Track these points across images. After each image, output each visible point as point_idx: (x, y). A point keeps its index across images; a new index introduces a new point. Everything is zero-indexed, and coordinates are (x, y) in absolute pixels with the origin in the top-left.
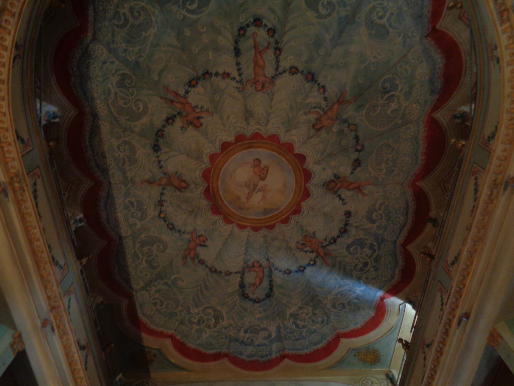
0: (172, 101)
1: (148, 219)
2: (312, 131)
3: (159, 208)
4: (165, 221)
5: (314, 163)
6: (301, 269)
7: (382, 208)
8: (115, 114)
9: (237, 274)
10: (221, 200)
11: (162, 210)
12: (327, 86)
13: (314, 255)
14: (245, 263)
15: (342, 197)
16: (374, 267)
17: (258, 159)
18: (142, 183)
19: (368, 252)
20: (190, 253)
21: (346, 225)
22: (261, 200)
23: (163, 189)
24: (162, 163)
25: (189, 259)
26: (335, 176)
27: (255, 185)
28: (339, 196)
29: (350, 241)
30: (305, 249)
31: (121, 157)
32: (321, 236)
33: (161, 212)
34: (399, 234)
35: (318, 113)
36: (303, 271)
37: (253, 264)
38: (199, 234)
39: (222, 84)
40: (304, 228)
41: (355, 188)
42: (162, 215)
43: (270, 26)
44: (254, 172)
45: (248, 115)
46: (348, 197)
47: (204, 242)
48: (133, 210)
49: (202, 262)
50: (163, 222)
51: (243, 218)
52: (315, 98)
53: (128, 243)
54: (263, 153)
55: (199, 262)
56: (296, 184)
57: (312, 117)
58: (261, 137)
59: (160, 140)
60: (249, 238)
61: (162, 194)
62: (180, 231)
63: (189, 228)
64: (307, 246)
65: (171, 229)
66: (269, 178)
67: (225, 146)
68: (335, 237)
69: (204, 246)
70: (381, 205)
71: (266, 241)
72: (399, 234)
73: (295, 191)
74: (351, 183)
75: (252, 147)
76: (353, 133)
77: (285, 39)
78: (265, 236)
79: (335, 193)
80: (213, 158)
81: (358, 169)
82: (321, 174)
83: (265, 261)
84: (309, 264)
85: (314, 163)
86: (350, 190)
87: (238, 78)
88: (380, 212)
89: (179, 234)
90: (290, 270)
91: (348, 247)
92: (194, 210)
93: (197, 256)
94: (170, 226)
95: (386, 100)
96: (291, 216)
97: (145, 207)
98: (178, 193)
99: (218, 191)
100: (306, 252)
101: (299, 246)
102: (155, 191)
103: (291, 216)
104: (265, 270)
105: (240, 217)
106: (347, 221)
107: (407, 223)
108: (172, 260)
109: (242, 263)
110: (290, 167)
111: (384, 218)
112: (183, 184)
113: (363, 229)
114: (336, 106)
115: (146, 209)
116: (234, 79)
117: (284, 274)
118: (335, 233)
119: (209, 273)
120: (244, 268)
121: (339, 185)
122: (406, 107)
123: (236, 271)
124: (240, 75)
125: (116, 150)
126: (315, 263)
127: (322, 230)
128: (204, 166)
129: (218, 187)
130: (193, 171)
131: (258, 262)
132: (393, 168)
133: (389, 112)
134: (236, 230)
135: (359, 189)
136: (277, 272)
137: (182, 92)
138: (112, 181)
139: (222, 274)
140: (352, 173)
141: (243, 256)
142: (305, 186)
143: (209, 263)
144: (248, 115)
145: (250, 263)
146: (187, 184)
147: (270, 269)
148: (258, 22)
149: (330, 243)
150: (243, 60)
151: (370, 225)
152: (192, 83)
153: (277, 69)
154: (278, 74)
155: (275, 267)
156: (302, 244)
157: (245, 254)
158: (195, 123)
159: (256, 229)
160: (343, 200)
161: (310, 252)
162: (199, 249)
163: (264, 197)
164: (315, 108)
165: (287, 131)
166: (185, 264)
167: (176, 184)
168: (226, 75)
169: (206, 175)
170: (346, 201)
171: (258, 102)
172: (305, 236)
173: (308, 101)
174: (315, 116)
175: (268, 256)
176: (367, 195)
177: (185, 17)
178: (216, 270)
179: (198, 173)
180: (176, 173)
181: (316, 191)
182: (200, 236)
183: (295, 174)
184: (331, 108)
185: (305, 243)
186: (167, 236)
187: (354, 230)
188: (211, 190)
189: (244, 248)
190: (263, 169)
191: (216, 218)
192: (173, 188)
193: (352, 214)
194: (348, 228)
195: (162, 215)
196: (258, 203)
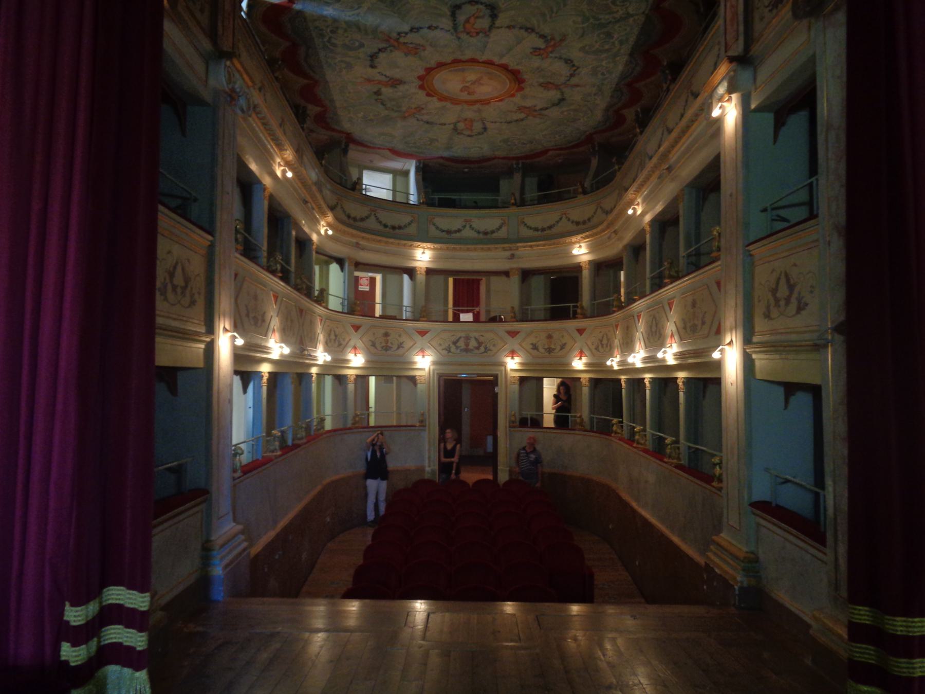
54: (465, 96)
172: (416, 54)
186: (576, 55)
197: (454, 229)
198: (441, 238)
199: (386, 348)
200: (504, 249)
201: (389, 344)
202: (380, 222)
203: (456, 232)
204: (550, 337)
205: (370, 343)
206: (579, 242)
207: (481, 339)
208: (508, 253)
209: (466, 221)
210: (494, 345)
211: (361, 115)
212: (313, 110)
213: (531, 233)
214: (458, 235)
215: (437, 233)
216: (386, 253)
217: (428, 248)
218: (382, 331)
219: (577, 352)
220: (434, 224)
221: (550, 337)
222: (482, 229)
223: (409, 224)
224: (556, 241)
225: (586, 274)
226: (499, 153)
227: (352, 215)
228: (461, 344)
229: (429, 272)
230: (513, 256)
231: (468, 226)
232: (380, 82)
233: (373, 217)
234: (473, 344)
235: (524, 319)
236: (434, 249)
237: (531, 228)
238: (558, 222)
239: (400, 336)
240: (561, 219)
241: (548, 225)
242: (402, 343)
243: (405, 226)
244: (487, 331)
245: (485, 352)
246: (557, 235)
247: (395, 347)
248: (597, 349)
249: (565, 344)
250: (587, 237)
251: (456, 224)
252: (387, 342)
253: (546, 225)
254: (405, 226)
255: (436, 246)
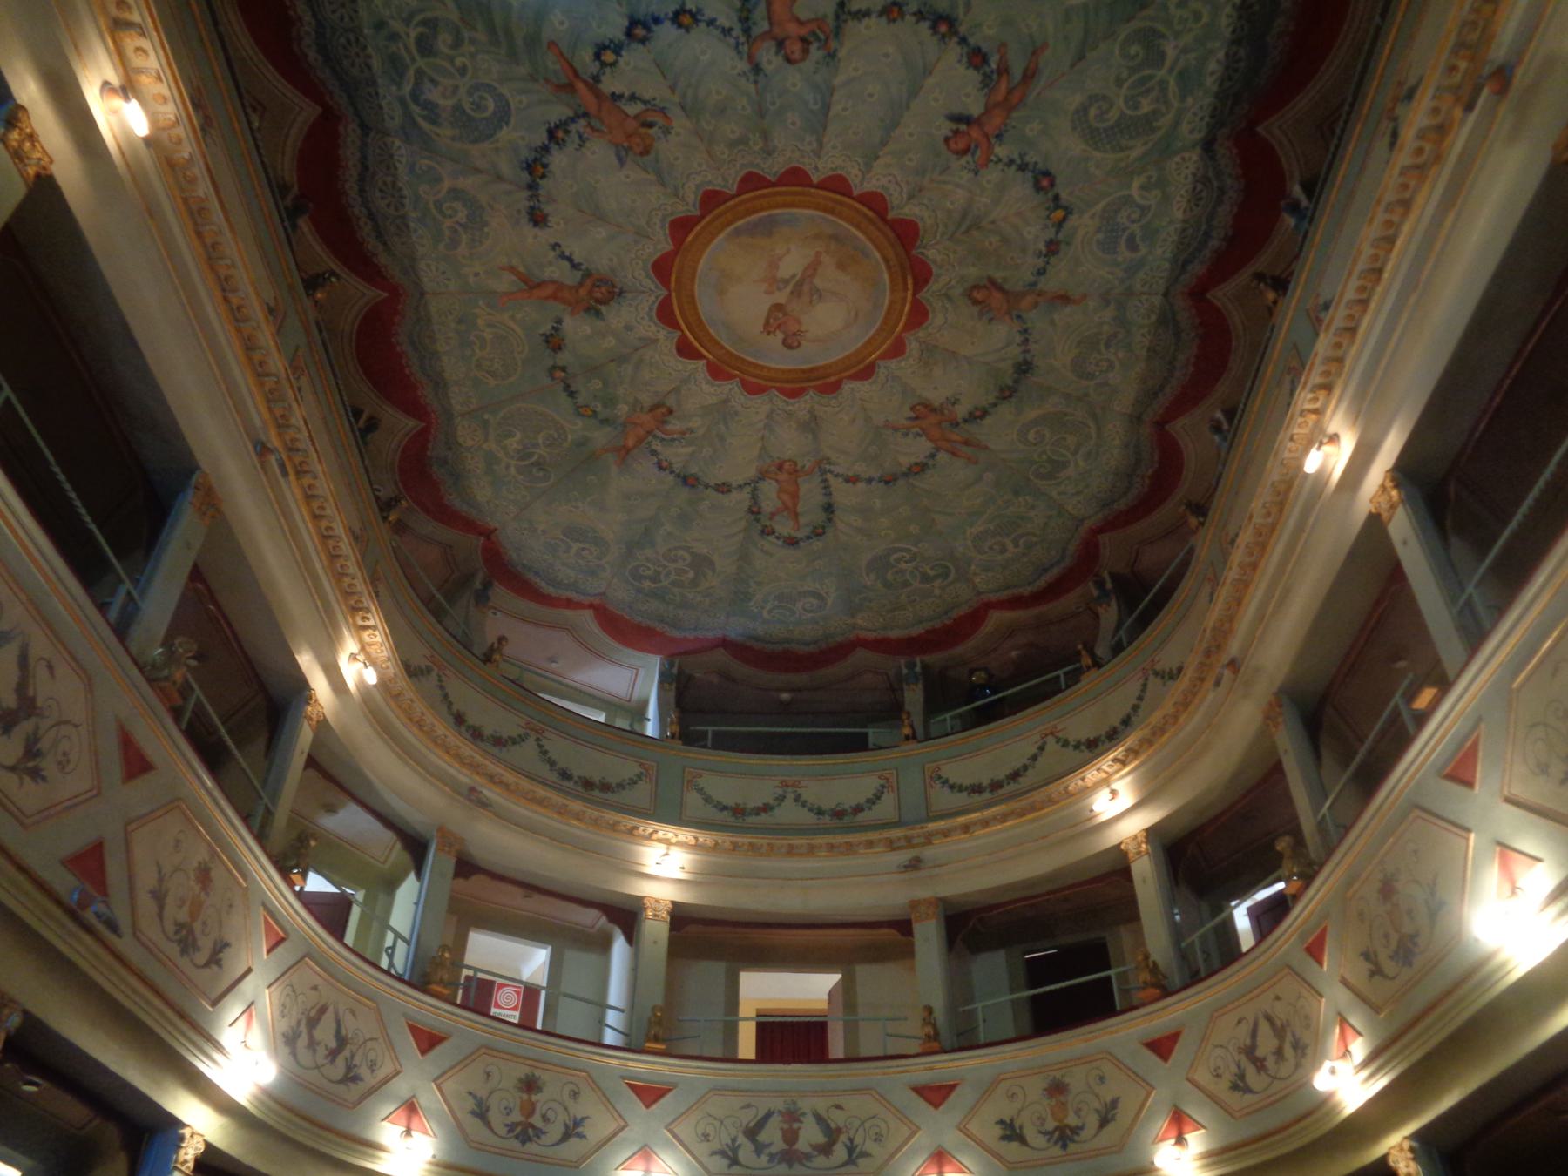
0: (966, 443)
1: (1103, 203)
2: (671, 402)
3: (1061, 236)
4: (1056, 198)
5: (656, 341)
6: (640, 32)
7: (447, 233)
8: (1092, 425)
9: (864, 7)
10: (886, 261)
11: (1053, 230)
12: (656, 470)
13: (609, 85)
14: (832, 55)
15: (566, 264)
16: (394, 37)
17: (790, 347)
18: (1084, 297)
19: (433, 95)
20: (1010, 92)
21: (532, 187)
22: (780, 259)
23: (1034, 284)
24: (1018, 339)
25: (1017, 72)
26: (598, 314)
27: (797, 292)
28: (575, 266)
29: (505, 134)
30: (639, 107)
31: (1112, 350)
32: (599, 151)
33: (1060, 225)
34: (364, 158)
35: (665, 433)
36: (634, 22)
37: (806, 52)
38: (968, 158)
39: (860, 468)
40: (652, 177)
41: (539, 285)
42: (1060, 214)
43: (771, 538)
44: (799, 323)
45: (811, 425)
46: (550, 263)
47: (956, 132)
48: (1135, 228)
49: (977, 58)
50: (1063, 195)
51: (832, 212)
52: (677, 454)
53: (1192, 129)
54: (775, 357)
55: (985, 59)
56: (693, 297)
57: (675, 425)
58: (782, 391)
59: (1010, 383)
60: (815, 145)
61: (1041, 272)
62: (1023, 167)
63: (992, 175)
64: (636, 117)
65: (1047, 174)
66: (765, 307)
67: (867, 373)
68: (554, 148)
69: (957, 118)
70: (454, 243)
71: (765, 136)
72: (364, 158)
73: (692, 280)
74: (554, 297)
75: (803, 371)
76: (581, 400)
77: (743, 523)
78: (769, 152)
79: (588, 274)
80: (897, 350)
81: (546, 328)
82: (634, 316)
83: (764, 65)
84: (617, 50)
85: (656, 341)
86: (553, 282)
87: (829, 476)
88: (448, 223)
89: (1027, 159)
90: (680, 26)
91: (503, 115)
92: (967, 232)
93: (987, 82)
94: (1045, 183)
95: (531, 455)
96: (697, 213)
97: (1100, 236)
98: (998, 275)
99: (892, 280)
100: (633, 98)
101: (660, 120)
102: (1059, 277)
103: (697, 213)
104: (765, 26)
105: (840, 215)
106: (535, 197)
107: (356, 188)
108: (1073, 66)
109: (842, 54)
110: (712, 332)
111: (432, 206)
112: (978, 296)
113: (481, 172)
114: (630, 443)
115: (1098, 230)
116: (837, 476)
117: (700, 11)
118: (558, 160)
119: (961, 11)
120: (838, 32)
121: (583, 292)
122: (486, 440)
123: (866, 21)
124: (825, 481)
125: (1117, 364)
126: (597, 56)
127: (592, 166)
128: (921, 334)
129: (893, 291)
130: (950, 323)
131: (789, 60)
132: (463, 328)
133: (519, 435)
134: (853, 174)
135: (531, 284)
136: (723, 21)
137: (942, 457)
138: (1157, 300)
139: (913, 7)
140: (560, 321)
141: (837, 81)
142: (668, 288)
143: (954, 51)
144: (811, 425)
145: (816, 53)
146: (970, 297)
147: (747, 31)
148: (792, 542)
149: (563, 125)
150: (819, 499)
151: (468, 183)
152: (921, 468)
153: (755, 489)
154: (753, 485)
155: (732, 41)
156: (650, 125)
157: (832, 90)
158: (924, 412)
159: (795, 176)
160: (563, 256)
161: (621, 96)
162: (976, 110)
163: (774, 265)
164: (673, 440)
165: (726, 401)
166: (1034, 53)
167: (997, 295)
168: (852, 480)
169: (919, 315)
170: (552, 254)
171: (790, 443)
172: (646, 152)
173: (690, 450)
174: (669, 427)
175: (756, 82)
176: (503, 269)
177: (916, 545)
178: (934, 28)
179: (937, 319)
180: (991, 320)
181: (637, 275)
182: (965, 151)
183: (701, 322)
184: (640, 441)
185: (643, 130)
186: (1065, 147)
187: (506, 168)
188: (910, 286)
189: (831, 114)
190: (779, 327)
191: (910, 211)
192: (1006, 287)
193: (524, 219)
194: (525, 177)
195: (1060, 214)
196: (788, 251)
197: (751, 805)
198: (722, 818)
199: (525, 1133)
200: (891, 845)
201: (536, 1120)
202: (552, 764)
203: (759, 811)
204: (1057, 1089)
205: (470, 1104)
206: (1106, 782)
207: (837, 1118)
208: (904, 856)
209: (784, 785)
210: (878, 1139)
211: (513, 443)
212: (398, 425)
213: (961, 799)
214: (764, 817)
215: (711, 813)
216: (557, 840)
217: (679, 844)
218: (522, 1071)
219: (1162, 1124)
220: (700, 791)
221: (1057, 1089)
222: (828, 804)
223: (633, 782)
224: (1038, 796)
225: (1144, 870)
226: (867, 624)
227: (471, 719)
228: (772, 1134)
229: (680, 917)
230: (915, 865)
231: (790, 797)
232: (557, 292)
233: (531, 741)
234: (810, 1135)
235: (966, 1041)
236: (696, 847)
237: (961, 789)
238: (1034, 758)
239: (575, 1095)
240: (1042, 748)
241: (1007, 771)
242: (578, 1123)
243: (621, 786)
244: (857, 1090)
245: (851, 1161)
246: (1034, 786)
247: (555, 1131)
248: (1239, 1085)
249: (1114, 1103)
250: (1133, 752)
251: (758, 791)
252: (529, 1109)
253: (1001, 774)
254: (621, 786)
255: (705, 838)
